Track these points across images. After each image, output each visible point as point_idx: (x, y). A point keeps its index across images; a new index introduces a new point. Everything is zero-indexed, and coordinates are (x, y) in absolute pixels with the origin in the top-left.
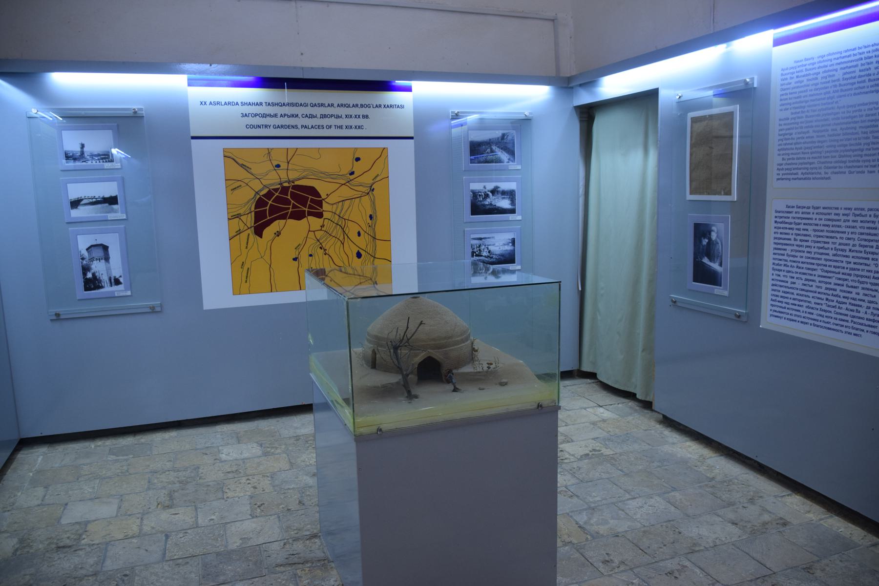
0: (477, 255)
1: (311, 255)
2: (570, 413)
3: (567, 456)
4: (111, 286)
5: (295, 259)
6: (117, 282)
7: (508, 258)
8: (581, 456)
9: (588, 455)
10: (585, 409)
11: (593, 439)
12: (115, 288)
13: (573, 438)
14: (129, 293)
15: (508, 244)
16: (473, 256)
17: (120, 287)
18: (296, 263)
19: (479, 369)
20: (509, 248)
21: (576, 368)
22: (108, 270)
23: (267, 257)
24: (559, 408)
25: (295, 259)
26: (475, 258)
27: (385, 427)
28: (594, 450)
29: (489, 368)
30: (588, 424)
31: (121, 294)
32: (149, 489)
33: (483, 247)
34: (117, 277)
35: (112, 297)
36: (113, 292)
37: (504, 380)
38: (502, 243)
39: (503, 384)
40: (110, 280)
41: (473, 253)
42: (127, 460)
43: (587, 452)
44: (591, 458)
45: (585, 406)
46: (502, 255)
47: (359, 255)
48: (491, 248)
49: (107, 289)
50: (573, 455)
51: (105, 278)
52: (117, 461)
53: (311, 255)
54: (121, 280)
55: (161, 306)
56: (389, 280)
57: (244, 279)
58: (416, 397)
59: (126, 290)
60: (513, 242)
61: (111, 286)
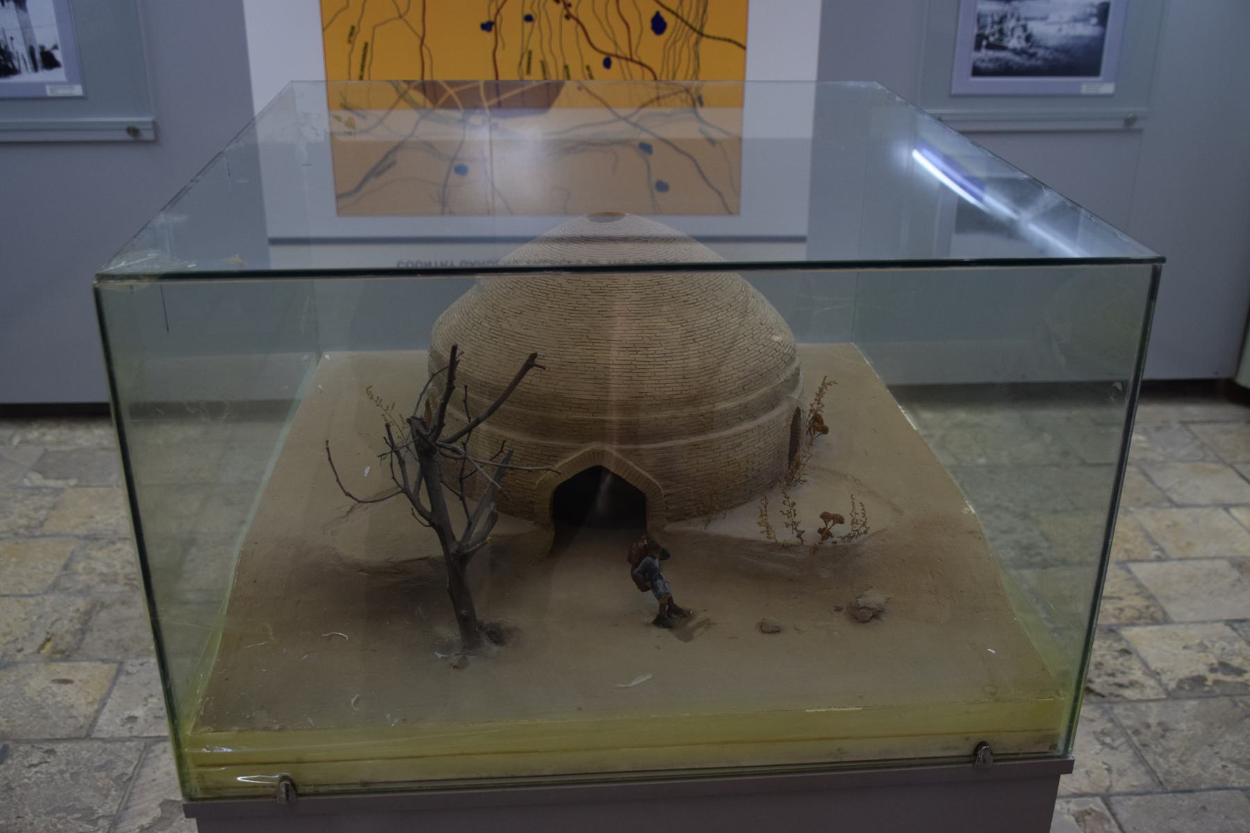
0: (990, 46)
1: (529, 18)
2: (1181, 516)
3: (1137, 674)
4: (36, 69)
5: (487, 27)
6: (49, 61)
7: (1080, 60)
8: (1181, 683)
9: (1199, 681)
10: (1227, 507)
11: (1230, 623)
12: (44, 76)
13: (1172, 609)
14: (78, 90)
15: (1085, 19)
16: (978, 47)
17: (58, 75)
18: (489, 37)
19: (785, 535)
20: (1088, 30)
21: (1223, 375)
22: (26, 28)
23: (414, 16)
24: (1068, 767)
25: (487, 27)
26: (985, 54)
27: (308, 775)
28: (1225, 667)
29: (825, 533)
30: (1222, 565)
31: (61, 92)
32: (54, 587)
33: (1011, 23)
34: (48, 47)
35: (37, 99)
36: (42, 85)
37: (874, 598)
38: (1067, 15)
39: (864, 616)
40: (31, 52)
41: (980, 38)
42: (57, 491)
43: (1202, 670)
44: (1210, 695)
45: (1228, 497)
46: (1063, 50)
47: (658, 25)
48: (1036, 28)
49: (28, 77)
50: (1155, 674)
51: (19, 48)
52: (36, 490)
53: (529, 18)
54: (58, 55)
55: (155, 126)
56: (736, 99)
57: (356, 71)
58: (498, 636)
59: (71, 81)
60: (1103, 14)
61: (36, 69)
